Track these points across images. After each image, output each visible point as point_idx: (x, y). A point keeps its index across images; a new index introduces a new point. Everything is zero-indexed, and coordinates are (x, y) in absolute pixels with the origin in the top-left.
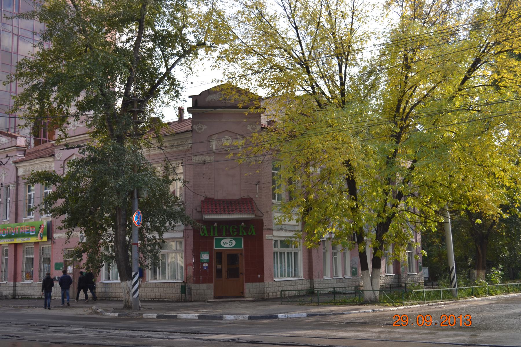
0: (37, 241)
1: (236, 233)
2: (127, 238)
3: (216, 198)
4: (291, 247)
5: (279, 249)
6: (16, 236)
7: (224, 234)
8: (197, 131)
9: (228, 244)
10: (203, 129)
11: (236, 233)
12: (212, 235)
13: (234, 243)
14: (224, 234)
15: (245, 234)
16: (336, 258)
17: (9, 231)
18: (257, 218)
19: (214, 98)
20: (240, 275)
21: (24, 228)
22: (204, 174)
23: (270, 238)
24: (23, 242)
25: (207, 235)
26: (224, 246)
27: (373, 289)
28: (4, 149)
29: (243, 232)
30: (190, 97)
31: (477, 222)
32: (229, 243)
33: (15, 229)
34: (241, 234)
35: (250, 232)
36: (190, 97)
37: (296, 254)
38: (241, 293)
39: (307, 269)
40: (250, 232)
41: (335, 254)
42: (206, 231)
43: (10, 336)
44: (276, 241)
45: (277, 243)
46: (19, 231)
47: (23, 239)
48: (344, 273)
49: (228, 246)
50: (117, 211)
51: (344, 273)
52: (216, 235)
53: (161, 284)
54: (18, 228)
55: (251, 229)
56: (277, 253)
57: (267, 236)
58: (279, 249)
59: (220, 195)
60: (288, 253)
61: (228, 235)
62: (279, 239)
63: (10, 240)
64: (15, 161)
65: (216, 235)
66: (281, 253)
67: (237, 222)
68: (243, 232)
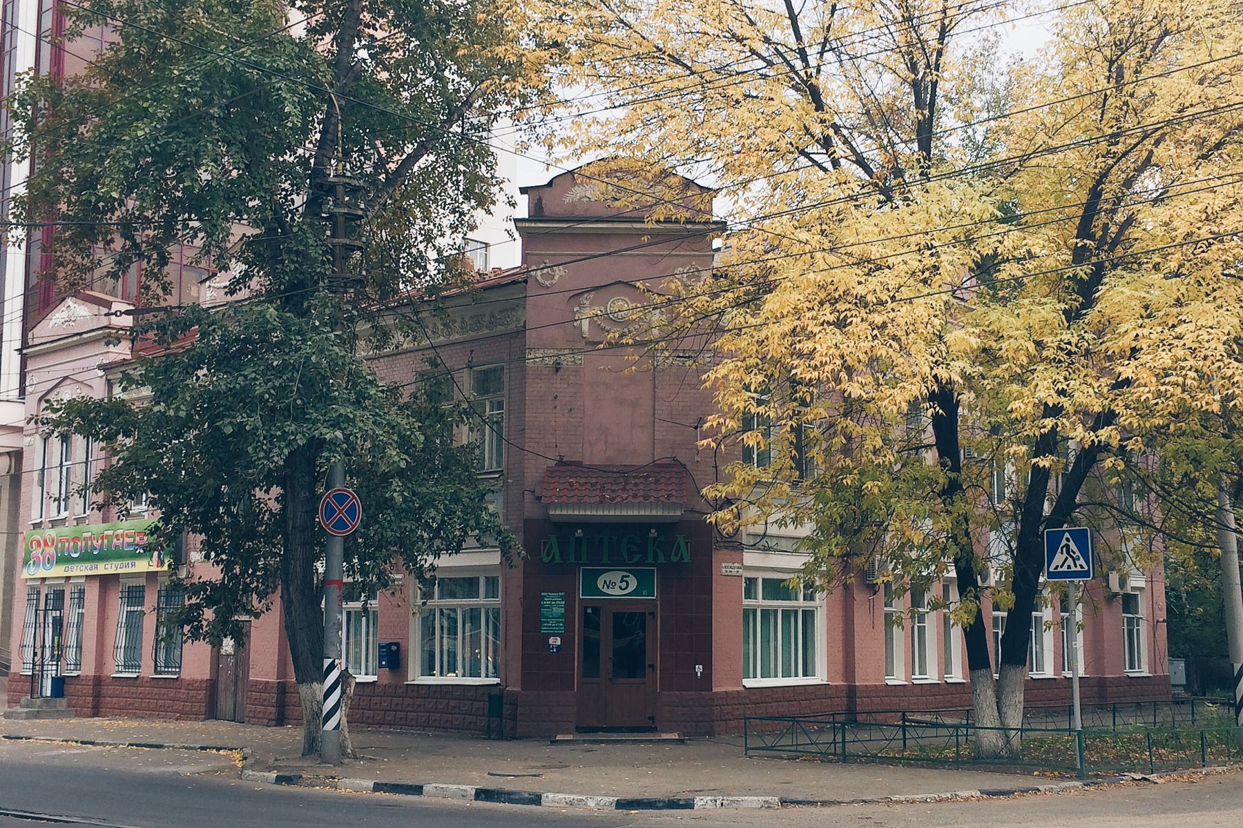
0: (151, 569)
1: (637, 558)
2: (320, 567)
3: (586, 463)
4: (796, 599)
5: (760, 602)
6: (103, 557)
7: (605, 560)
8: (542, 281)
9: (617, 587)
10: (556, 278)
11: (637, 558)
12: (572, 559)
13: (633, 583)
14: (605, 560)
15: (661, 560)
16: (922, 630)
17: (86, 544)
18: (691, 517)
19: (588, 194)
20: (648, 670)
21: (122, 535)
22: (556, 397)
23: (734, 572)
24: (119, 571)
25: (558, 560)
26: (605, 590)
27: (1002, 723)
28: (80, 334)
29: (656, 556)
30: (524, 191)
31: (518, 689)
32: (619, 584)
33: (102, 538)
34: (651, 560)
35: (676, 555)
36: (524, 191)
37: (808, 616)
38: (649, 718)
39: (840, 656)
40: (676, 555)
41: (921, 618)
42: (556, 549)
43: (32, 818)
44: (751, 582)
45: (756, 586)
46: (110, 543)
47: (118, 563)
48: (946, 666)
49: (616, 592)
50: (288, 489)
51: (946, 666)
52: (584, 560)
53: (416, 688)
54: (107, 536)
55: (679, 546)
56: (755, 611)
57: (724, 567)
58: (760, 602)
59: (594, 455)
60: (787, 614)
61: (616, 563)
62: (760, 576)
63: (89, 565)
64: (106, 364)
65: (584, 560)
66: (766, 613)
67: (638, 528)
68: (656, 556)
